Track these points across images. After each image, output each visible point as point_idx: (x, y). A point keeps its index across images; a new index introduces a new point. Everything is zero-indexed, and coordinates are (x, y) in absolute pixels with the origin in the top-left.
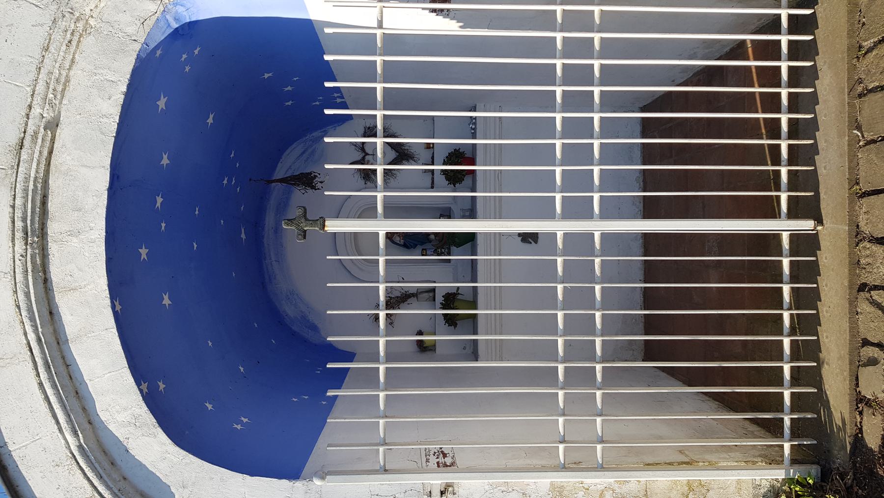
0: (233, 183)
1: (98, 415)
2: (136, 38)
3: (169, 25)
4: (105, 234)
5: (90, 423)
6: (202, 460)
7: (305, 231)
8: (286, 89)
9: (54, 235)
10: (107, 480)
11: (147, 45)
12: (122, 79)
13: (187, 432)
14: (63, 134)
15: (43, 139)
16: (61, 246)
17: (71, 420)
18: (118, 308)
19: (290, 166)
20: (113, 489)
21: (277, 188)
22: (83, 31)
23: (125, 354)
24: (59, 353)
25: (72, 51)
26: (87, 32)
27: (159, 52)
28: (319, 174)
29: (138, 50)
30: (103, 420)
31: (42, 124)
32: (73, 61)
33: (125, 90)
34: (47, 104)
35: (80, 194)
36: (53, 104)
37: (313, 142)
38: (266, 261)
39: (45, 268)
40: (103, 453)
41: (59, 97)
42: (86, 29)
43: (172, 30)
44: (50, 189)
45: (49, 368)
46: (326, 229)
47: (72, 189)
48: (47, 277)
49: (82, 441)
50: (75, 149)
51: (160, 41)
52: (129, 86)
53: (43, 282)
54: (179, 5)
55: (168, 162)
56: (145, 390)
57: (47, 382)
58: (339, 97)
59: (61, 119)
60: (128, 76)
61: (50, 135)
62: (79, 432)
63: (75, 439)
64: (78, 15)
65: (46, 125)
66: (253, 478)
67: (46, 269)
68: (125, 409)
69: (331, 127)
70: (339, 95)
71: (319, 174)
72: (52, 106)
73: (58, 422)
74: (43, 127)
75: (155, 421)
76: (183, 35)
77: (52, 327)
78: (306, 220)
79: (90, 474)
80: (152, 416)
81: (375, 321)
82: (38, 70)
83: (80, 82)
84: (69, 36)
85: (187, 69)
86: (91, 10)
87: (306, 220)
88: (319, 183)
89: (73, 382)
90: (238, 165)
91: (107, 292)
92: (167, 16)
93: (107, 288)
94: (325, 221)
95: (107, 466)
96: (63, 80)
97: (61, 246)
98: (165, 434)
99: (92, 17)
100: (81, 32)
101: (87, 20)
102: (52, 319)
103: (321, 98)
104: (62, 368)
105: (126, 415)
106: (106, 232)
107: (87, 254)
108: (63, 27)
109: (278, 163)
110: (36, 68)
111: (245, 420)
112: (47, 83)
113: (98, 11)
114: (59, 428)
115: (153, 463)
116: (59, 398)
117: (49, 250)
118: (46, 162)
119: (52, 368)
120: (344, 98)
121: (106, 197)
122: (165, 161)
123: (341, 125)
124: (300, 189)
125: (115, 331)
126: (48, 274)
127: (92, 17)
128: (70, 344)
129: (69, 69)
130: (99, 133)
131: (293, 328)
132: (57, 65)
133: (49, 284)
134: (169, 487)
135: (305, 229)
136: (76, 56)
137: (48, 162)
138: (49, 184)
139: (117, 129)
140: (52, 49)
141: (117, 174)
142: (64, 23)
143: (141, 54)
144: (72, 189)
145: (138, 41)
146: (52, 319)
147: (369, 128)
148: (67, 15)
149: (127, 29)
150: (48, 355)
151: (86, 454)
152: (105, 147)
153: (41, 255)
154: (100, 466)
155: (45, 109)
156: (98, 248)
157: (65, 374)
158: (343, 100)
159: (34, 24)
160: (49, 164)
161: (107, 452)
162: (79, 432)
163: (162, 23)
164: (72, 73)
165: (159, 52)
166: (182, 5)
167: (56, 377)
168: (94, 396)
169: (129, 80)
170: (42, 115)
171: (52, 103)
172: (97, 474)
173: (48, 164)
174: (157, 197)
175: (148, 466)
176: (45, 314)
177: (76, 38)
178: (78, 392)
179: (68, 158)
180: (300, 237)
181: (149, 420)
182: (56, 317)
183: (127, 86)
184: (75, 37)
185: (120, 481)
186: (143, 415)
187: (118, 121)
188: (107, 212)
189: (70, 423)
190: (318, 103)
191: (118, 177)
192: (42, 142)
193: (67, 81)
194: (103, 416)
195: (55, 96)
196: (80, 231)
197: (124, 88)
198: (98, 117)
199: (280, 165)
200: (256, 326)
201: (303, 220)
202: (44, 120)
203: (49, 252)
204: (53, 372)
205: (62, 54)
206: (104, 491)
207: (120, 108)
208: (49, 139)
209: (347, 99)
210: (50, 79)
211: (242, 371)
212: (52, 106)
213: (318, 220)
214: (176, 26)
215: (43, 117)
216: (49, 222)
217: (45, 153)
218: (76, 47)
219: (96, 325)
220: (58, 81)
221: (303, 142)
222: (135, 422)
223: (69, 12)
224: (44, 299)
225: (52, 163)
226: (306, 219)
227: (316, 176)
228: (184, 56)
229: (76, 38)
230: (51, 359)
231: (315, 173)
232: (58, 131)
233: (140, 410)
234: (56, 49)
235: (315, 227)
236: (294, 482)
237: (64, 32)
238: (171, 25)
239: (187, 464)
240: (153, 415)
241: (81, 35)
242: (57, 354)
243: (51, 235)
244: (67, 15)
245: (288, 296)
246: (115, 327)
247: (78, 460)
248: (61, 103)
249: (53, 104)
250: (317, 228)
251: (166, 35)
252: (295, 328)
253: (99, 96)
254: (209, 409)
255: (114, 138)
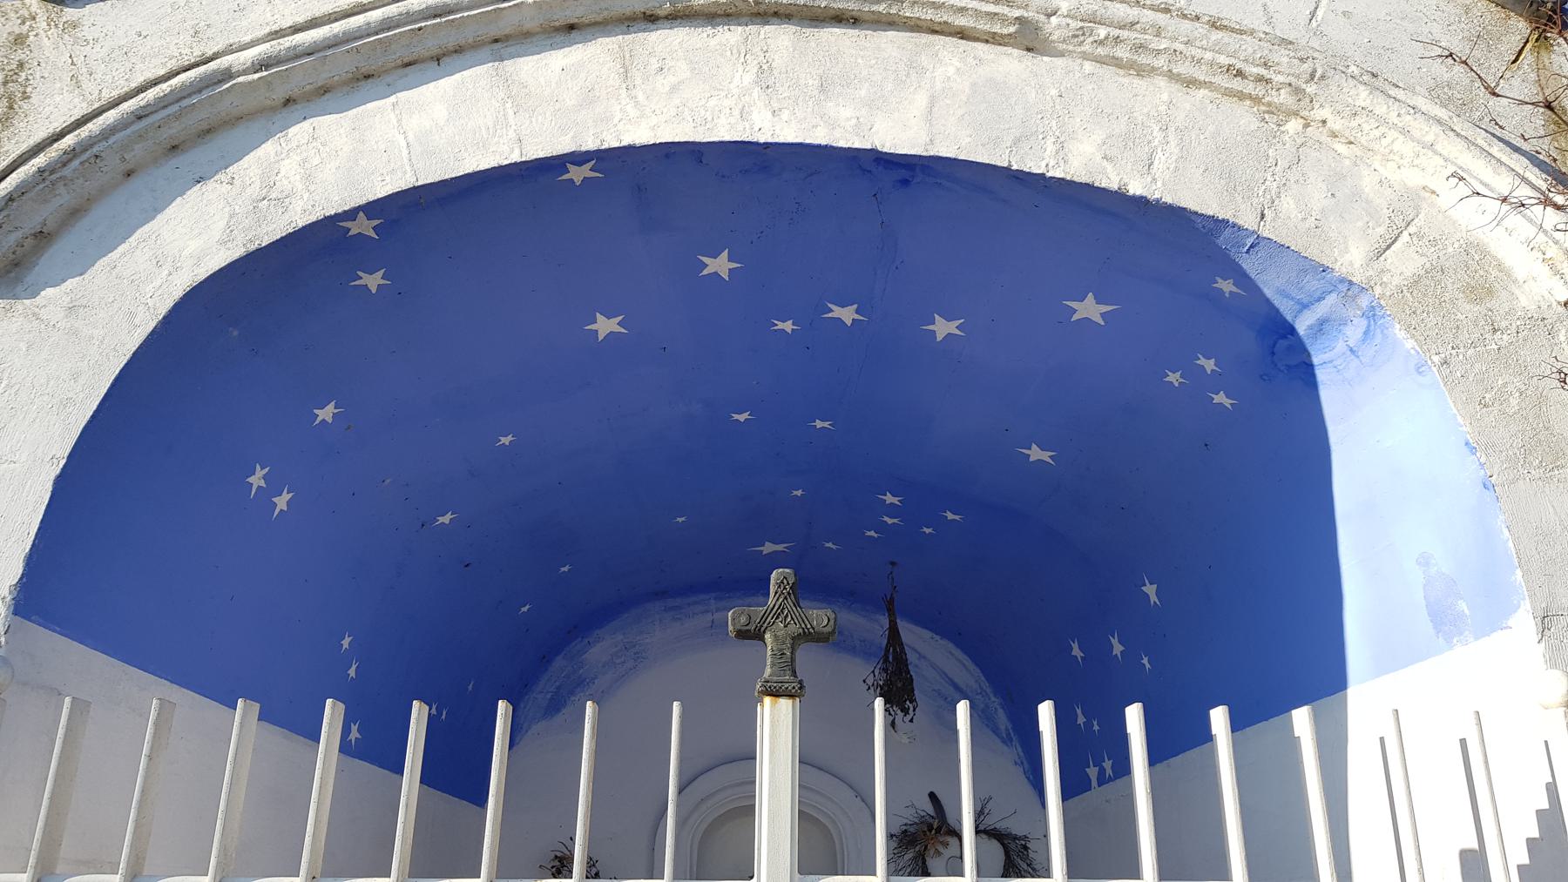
0: (886, 519)
1: (305, 118)
2: (1268, 218)
3: (1305, 306)
4: (762, 140)
5: (288, 102)
6: (134, 354)
7: (758, 636)
8: (1115, 641)
9: (762, 36)
10: (128, 131)
11: (1251, 247)
12: (1159, 184)
13: (236, 333)
14: (1010, 64)
15: (996, 14)
16: (735, 51)
17: (297, 57)
18: (577, 174)
19: (924, 657)
20: (105, 143)
21: (875, 628)
22: (1269, 104)
23: (452, 179)
24: (470, 40)
25: (1218, 80)
26: (1267, 116)
27: (1227, 286)
28: (911, 721)
29: (1240, 222)
30: (290, 130)
31: (1031, 14)
32: (1191, 83)
33: (1131, 192)
34: (1081, 24)
35: (863, 93)
36: (1082, 38)
37: (983, 711)
38: (713, 601)
39: (681, 18)
40: (205, 126)
41: (1101, 51)
42: (1273, 113)
43: (1289, 318)
44: (875, 33)
45: (435, 16)
46: (767, 700)
47: (874, 75)
48: (659, 22)
49: (241, 79)
50: (974, 85)
51: (1261, 286)
52: (1141, 202)
53: (648, 13)
54: (1369, 326)
55: (939, 338)
56: (355, 228)
57: (401, 10)
58: (1102, 771)
59: (1045, 58)
60: (1168, 199)
61: (1005, 31)
62: (265, 73)
63: (249, 64)
64: (1308, 90)
65: (1030, 22)
66: (51, 483)
67: (679, 21)
68: (308, 178)
69: (1022, 754)
70: (1109, 772)
71: (911, 721)
72: (1077, 36)
73: (296, 29)
74: (1026, 15)
75: (263, 245)
76: (1273, 353)
77: (539, 29)
78: (793, 638)
79: (151, 95)
80: (279, 237)
81: (556, 857)
82: (1163, 6)
83: (1139, 98)
84: (1255, 70)
85: (1174, 378)
86: (1324, 122)
87: (793, 638)
88: (892, 718)
89: (397, 67)
90: (927, 531)
91: (615, 144)
92: (1334, 295)
93: (625, 143)
94: (791, 696)
95: (174, 131)
96: (1143, 59)
97: (735, 51)
98: (223, 265)
99: (1306, 126)
100: (1267, 99)
101: (1296, 114)
102: (557, 30)
103: (1096, 728)
104: (431, 45)
105: (292, 179)
106: (767, 145)
107: (712, 102)
108: (1275, 58)
109: (931, 630)
110: (1166, 3)
111: (282, 502)
112: (1133, 24)
113: (1324, 139)
114: (284, 32)
115: (154, 236)
116: (357, 34)
117: (726, 28)
118: (940, 23)
119: (434, 21)
120: (1100, 785)
121: (857, 145)
122: (943, 328)
123: (1028, 778)
124: (877, 673)
125: (515, 157)
126: (668, 24)
127: (1306, 126)
128: (490, 64)
129: (1171, 76)
130: (1018, 135)
131: (559, 658)
132: (1179, 47)
133: (643, 25)
134: (81, 275)
135: (768, 636)
136: (1203, 92)
137: (937, 29)
138: (885, 31)
139: (1029, 173)
140: (1216, 35)
141: (913, 177)
142: (1285, 60)
143: (1228, 231)
144: (874, 75)
145: (1262, 223)
146: (557, 30)
147: (1026, 848)
148: (1307, 67)
149: (1288, 198)
150: (466, 14)
151: (207, 87)
152: (983, 145)
153: (713, 10)
154: (169, 115)
155: (1070, 21)
156: (728, 127)
157: (419, 51)
158: (1094, 783)
159: (1271, 8)
160: (935, 32)
161: (209, 137)
162: (265, 73)
163: (1313, 284)
164: (1162, 82)
165: (1227, 286)
166: (1366, 333)
167: (412, 30)
168: (354, 111)
169: (1158, 201)
170: (1054, 14)
171: (1083, 34)
172: (150, 109)
173: (934, 29)
174: (855, 306)
175: (146, 228)
176: (568, 13)
177: (1249, 87)
178: (370, 80)
179: (951, 70)
180: (743, 620)
181: (270, 229)
182: (559, 38)
183: (1142, 197)
184: (1251, 86)
185: (123, 160)
186: (286, 216)
187: (1049, 175)
188: (819, 146)
189: (291, 53)
190: (1081, 720)
191: (905, 182)
192: (988, 14)
193: (1142, 71)
194: (299, 132)
195: (1101, 43)
196: (770, 90)
197: (1135, 188)
198: (1057, 133)
199: (927, 634)
200: (563, 569)
201: (794, 629)
202: (1042, 18)
203: (720, 28)
204: (423, 24)
205: (1208, 56)
206: (101, 122)
207: (1083, 179)
208: (997, 28)
209: (1096, 795)
210: (1144, 31)
211: (441, 520)
212: (1077, 36)
213: (794, 673)
214: (1302, 327)
215: (1049, 16)
216: (792, 28)
217: (961, 21)
218: (1226, 89)
219: (533, 120)
220: (1140, 47)
221: (981, 688)
222: (270, 197)
223: (1315, 71)
224: (606, 13)
225: (937, 37)
226: (797, 640)
227: (905, 711)
228: (1209, 365)
229: (1249, 87)
230: (456, 19)
231: (914, 710)
232: (1016, 52)
233: (299, 209)
234: (1217, 43)
235: (773, 665)
236: (9, 598)
237: (1263, 60)
238: (1305, 311)
239: (132, 315)
240: (282, 238)
241: (1256, 100)
242: (468, 35)
243: (762, 32)
244: (1307, 67)
245: (635, 646)
246: (523, 159)
247: (194, 71)
248: (1085, 56)
249: (1082, 38)
250: (768, 671)
251: (1278, 302)
252: (559, 662)
253: (1109, 137)
254: (316, 411)
255: (1006, 165)
